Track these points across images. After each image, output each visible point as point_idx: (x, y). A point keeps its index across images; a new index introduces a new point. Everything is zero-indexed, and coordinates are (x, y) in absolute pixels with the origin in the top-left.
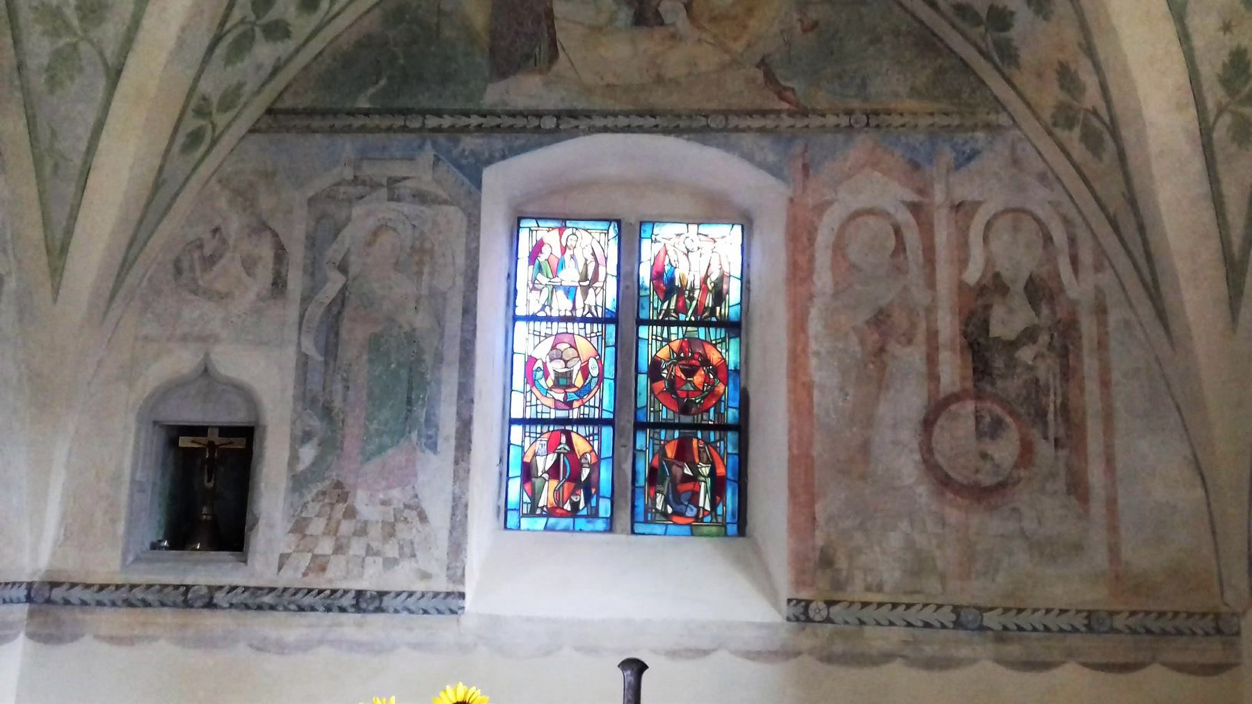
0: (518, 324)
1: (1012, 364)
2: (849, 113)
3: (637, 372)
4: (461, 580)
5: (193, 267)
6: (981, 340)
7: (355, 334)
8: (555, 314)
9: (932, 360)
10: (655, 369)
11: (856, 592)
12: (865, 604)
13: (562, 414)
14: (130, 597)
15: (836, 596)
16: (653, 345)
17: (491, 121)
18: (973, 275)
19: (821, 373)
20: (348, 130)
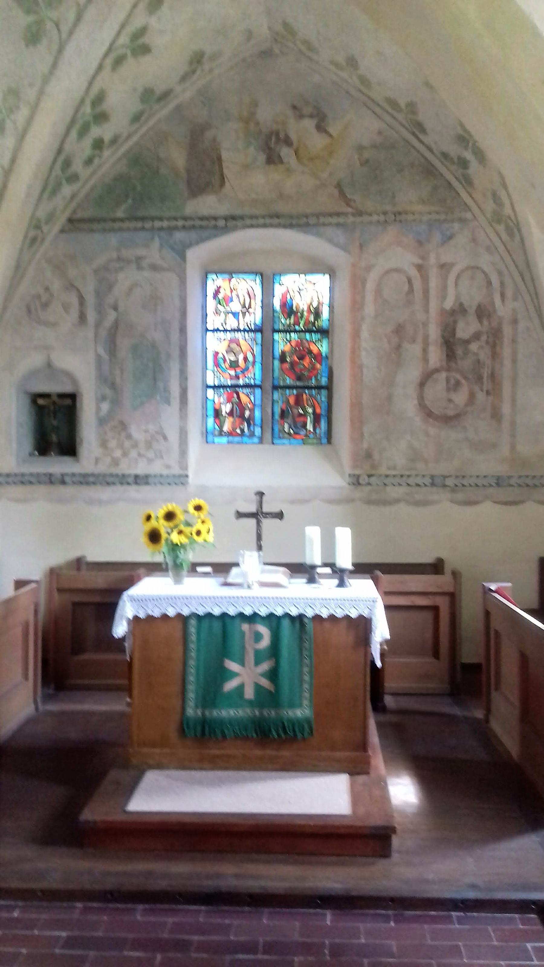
0: (209, 333)
1: (466, 352)
2: (385, 213)
3: (274, 358)
4: (186, 468)
5: (36, 309)
6: (451, 340)
7: (124, 344)
8: (229, 329)
9: (425, 351)
10: (283, 358)
11: (383, 470)
12: (387, 476)
13: (234, 382)
14: (22, 480)
15: (373, 472)
16: (281, 343)
17: (189, 223)
18: (449, 304)
19: (369, 360)
20: (112, 230)
